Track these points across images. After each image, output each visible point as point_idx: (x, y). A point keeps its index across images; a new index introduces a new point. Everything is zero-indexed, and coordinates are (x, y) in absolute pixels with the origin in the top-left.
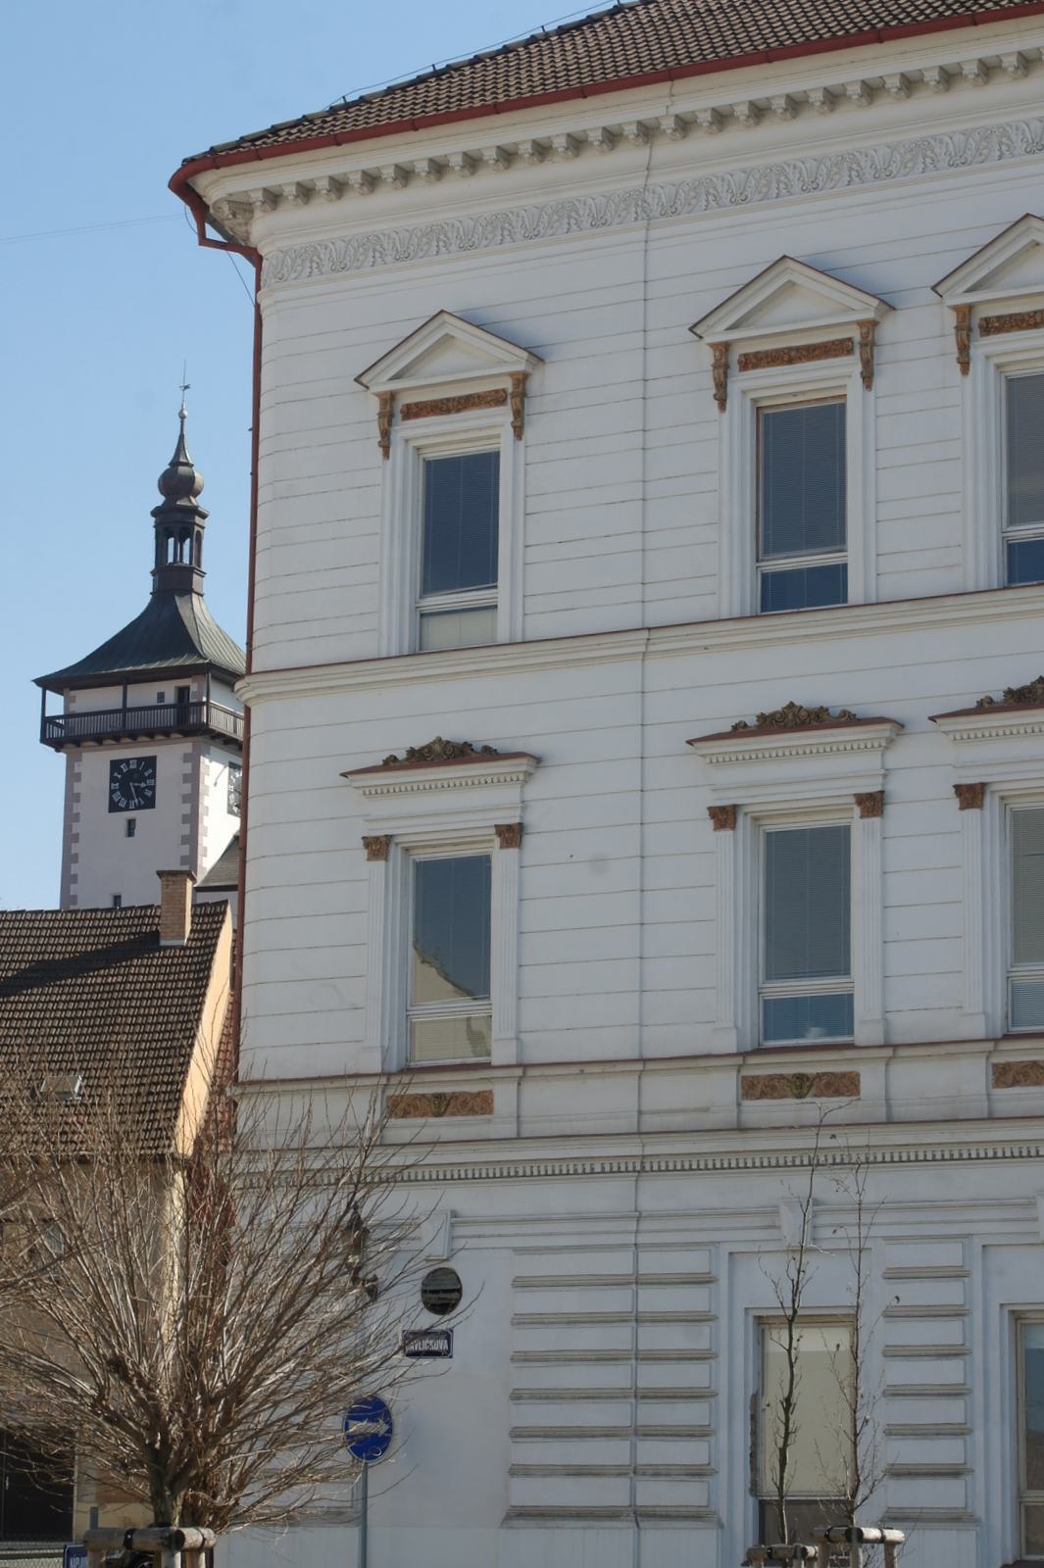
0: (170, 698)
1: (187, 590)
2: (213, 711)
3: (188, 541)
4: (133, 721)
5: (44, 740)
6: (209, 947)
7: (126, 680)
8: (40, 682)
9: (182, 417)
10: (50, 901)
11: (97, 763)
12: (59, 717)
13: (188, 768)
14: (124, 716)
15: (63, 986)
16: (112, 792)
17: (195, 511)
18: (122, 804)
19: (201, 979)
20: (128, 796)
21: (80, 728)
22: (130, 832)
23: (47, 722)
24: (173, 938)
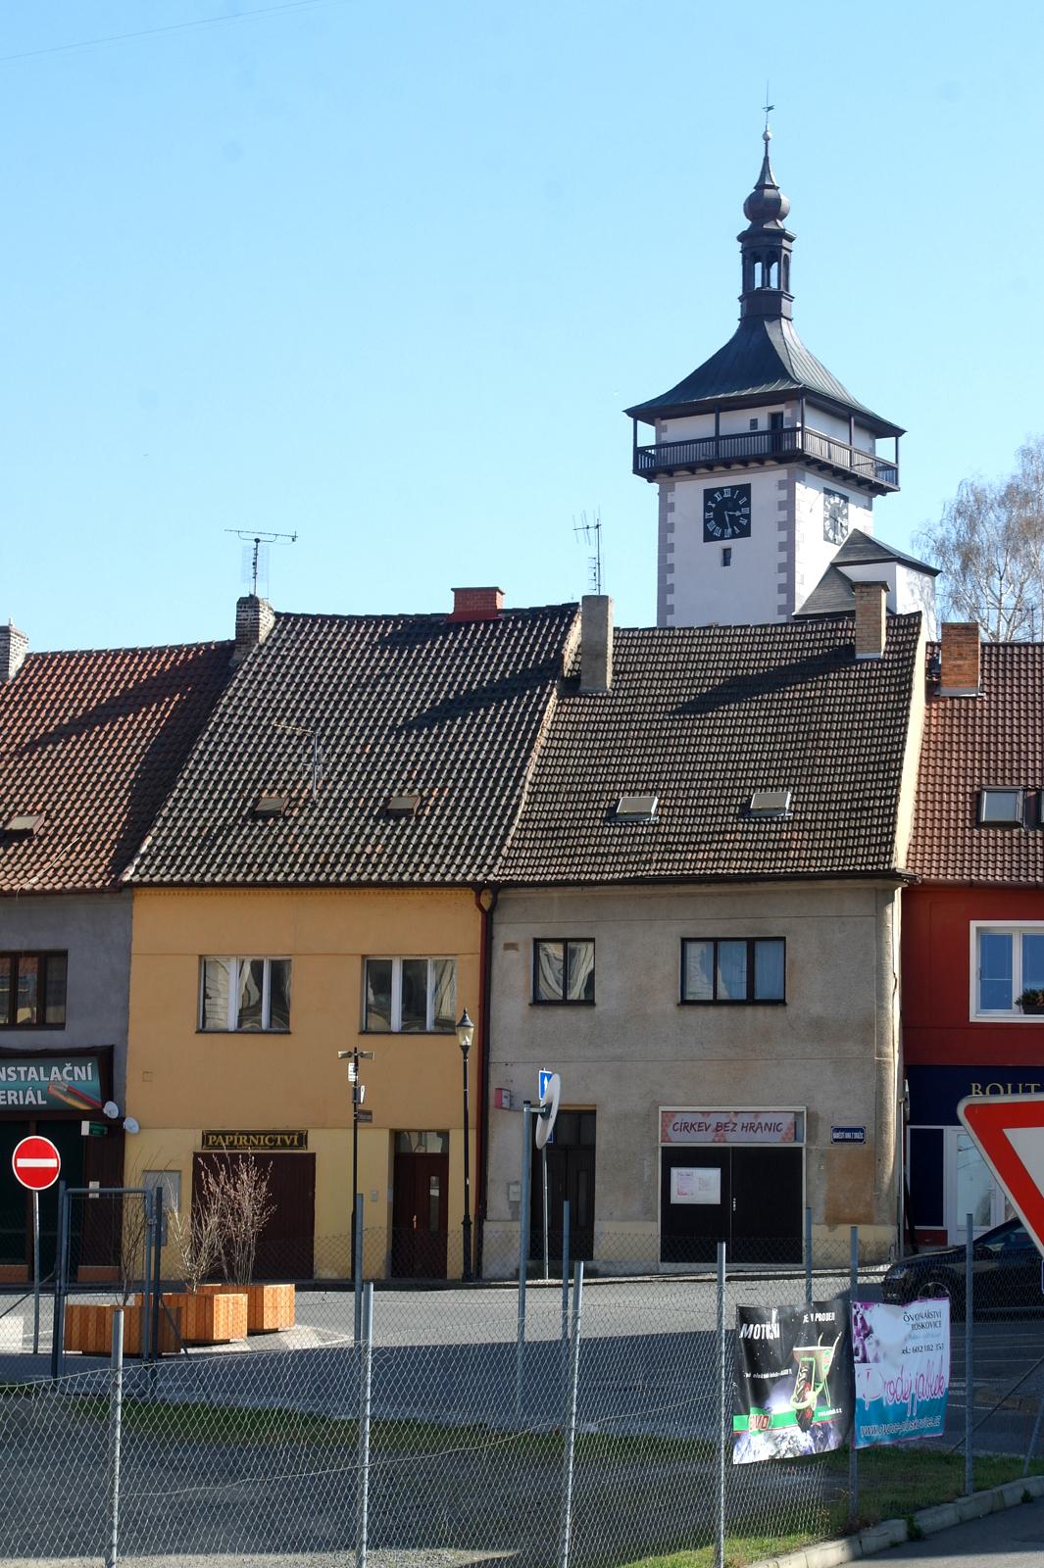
0: (764, 424)
1: (777, 315)
2: (809, 437)
3: (775, 265)
4: (727, 449)
5: (637, 471)
6: (907, 659)
7: (718, 408)
8: (631, 412)
9: (767, 139)
10: (651, 621)
11: (691, 493)
12: (651, 447)
13: (783, 495)
14: (717, 445)
15: (761, 701)
16: (706, 521)
17: (782, 234)
18: (717, 534)
19: (904, 692)
20: (722, 524)
21: (672, 457)
22: (726, 562)
23: (639, 452)
24: (869, 651)
